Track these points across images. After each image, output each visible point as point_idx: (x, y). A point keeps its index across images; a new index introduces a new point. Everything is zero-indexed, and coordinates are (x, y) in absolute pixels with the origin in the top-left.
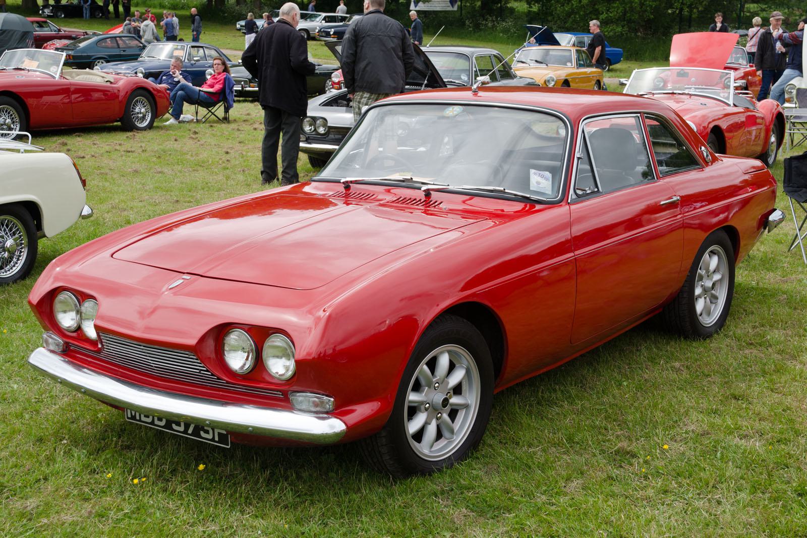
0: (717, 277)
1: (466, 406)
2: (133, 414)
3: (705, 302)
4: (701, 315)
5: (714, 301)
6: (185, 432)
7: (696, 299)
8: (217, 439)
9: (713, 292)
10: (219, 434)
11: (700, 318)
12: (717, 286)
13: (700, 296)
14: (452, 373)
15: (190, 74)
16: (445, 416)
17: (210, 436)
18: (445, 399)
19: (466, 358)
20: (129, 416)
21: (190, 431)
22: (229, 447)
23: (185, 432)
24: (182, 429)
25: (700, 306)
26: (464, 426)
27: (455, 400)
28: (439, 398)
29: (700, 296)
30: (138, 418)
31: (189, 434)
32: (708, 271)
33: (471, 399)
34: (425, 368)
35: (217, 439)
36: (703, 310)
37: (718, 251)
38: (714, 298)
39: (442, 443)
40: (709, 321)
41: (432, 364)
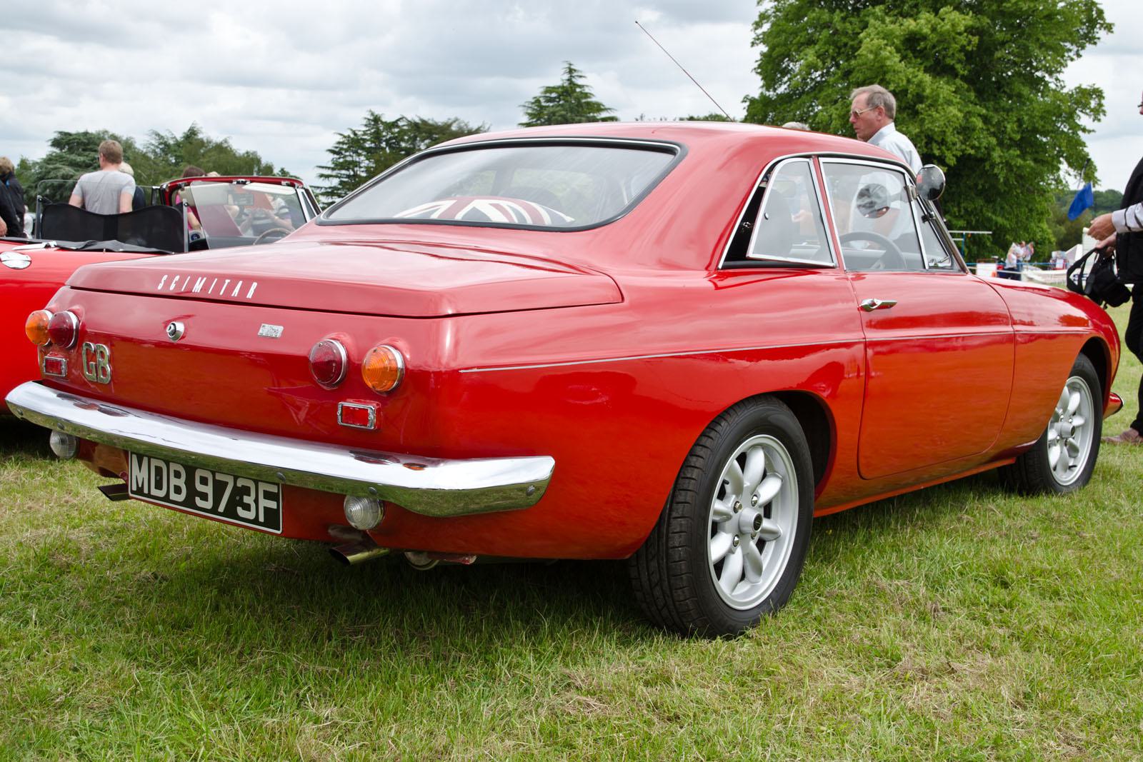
0: (1078, 421)
2: (140, 486)
5: (1074, 455)
8: (261, 519)
11: (1054, 473)
12: (1078, 434)
14: (760, 480)
16: (753, 544)
17: (250, 515)
18: (753, 508)
20: (134, 488)
21: (221, 509)
22: (279, 532)
25: (1055, 455)
26: (776, 562)
29: (1054, 442)
30: (146, 491)
32: (1065, 409)
33: (785, 525)
34: (736, 464)
35: (261, 519)
36: (1057, 463)
37: (1081, 386)
38: (1073, 450)
39: (743, 587)
40: (1066, 478)
41: (742, 460)
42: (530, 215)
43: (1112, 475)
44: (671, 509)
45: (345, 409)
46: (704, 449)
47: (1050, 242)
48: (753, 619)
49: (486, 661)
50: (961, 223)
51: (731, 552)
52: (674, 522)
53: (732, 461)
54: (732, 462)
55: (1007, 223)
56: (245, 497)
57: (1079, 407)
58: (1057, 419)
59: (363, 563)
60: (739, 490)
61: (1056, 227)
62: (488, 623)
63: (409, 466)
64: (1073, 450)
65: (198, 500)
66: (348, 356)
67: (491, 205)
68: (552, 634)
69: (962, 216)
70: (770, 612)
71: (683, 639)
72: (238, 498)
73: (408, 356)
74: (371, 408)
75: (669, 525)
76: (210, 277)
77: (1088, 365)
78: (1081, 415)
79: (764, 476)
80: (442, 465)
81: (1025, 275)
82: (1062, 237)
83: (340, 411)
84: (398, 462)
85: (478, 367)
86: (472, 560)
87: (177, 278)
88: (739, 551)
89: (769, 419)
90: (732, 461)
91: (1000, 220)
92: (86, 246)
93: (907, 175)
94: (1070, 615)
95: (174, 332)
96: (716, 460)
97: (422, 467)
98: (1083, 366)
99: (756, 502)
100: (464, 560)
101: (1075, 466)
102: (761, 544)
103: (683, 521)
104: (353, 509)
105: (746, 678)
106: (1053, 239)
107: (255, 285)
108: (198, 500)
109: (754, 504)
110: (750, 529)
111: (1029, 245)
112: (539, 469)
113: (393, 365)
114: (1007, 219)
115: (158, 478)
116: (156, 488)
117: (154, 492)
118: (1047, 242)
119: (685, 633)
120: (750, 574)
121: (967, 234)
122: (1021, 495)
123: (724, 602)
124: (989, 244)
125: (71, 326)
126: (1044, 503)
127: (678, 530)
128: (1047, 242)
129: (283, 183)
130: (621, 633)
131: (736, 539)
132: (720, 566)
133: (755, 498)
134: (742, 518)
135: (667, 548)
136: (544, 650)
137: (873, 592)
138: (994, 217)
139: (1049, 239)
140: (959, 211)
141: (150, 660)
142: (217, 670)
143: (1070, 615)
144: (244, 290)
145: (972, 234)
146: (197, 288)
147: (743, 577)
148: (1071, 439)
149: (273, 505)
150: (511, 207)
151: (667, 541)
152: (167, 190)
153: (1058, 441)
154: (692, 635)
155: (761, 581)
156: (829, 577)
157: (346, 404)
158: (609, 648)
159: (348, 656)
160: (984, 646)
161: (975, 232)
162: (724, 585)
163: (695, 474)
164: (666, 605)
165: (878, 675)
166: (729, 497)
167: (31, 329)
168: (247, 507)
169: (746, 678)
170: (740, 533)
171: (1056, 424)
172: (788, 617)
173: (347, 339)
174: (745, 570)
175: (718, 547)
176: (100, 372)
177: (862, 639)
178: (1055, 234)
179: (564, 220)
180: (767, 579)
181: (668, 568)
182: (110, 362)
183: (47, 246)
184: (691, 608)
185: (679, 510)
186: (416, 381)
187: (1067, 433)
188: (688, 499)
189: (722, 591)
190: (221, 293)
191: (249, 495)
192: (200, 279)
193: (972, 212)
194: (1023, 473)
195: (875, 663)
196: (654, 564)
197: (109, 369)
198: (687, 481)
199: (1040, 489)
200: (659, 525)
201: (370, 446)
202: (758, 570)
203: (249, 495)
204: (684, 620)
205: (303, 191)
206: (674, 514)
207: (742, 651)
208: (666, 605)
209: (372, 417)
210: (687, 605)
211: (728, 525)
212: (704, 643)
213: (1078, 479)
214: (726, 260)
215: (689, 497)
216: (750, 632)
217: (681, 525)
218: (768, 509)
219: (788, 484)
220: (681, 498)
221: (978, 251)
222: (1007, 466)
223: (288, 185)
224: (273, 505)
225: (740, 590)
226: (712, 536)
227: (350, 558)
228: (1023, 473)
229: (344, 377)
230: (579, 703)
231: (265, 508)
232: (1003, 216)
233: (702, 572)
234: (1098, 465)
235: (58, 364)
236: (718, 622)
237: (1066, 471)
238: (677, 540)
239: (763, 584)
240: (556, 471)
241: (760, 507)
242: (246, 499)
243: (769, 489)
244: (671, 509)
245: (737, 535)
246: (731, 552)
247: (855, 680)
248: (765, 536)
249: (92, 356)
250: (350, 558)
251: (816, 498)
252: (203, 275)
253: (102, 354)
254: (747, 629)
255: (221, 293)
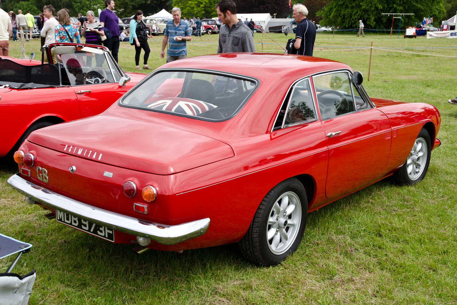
0: (420, 154)
1: (293, 225)
2: (61, 218)
3: (413, 167)
4: (410, 174)
6: (89, 230)
7: (408, 166)
8: (107, 236)
9: (418, 162)
10: (108, 233)
12: (421, 159)
13: (410, 164)
15: (83, 23)
16: (284, 230)
17: (103, 234)
18: (284, 222)
19: (296, 199)
20: (59, 219)
21: (92, 230)
22: (113, 242)
23: (89, 230)
24: (87, 228)
25: (410, 169)
26: (292, 235)
27: (289, 222)
28: (282, 220)
29: (410, 164)
30: (63, 220)
31: (91, 232)
32: (415, 150)
33: (296, 221)
34: (278, 204)
35: (107, 236)
39: (281, 245)
40: (414, 177)
41: (280, 202)
42: (199, 107)
43: (435, 171)
44: (253, 224)
45: (136, 206)
46: (265, 202)
47: (443, 12)
48: (284, 257)
49: (188, 281)
50: (401, 8)
51: (276, 234)
52: (254, 229)
53: (276, 203)
54: (276, 203)
55: (422, 7)
56: (100, 228)
57: (421, 148)
58: (412, 155)
59: (143, 253)
60: (279, 212)
61: (447, 4)
62: (188, 264)
63: (159, 227)
64: (418, 166)
65: (83, 226)
66: (137, 188)
67: (186, 104)
68: (210, 268)
69: (401, 5)
70: (290, 254)
71: (258, 268)
72: (98, 228)
73: (157, 189)
74: (145, 206)
75: (252, 229)
76: (84, 149)
77: (426, 132)
78: (422, 151)
79: (289, 204)
80: (171, 227)
81: (428, 34)
82: (449, 9)
83: (134, 207)
84: (155, 225)
85: (183, 192)
86: (182, 252)
87: (71, 147)
88: (279, 233)
89: (290, 186)
90: (276, 203)
91: (419, 6)
92: (22, 86)
93: (349, 73)
94: (401, 251)
95: (72, 170)
96: (269, 206)
97: (163, 228)
98: (423, 133)
99: (285, 215)
100: (179, 252)
101: (419, 172)
102: (287, 230)
103: (257, 229)
104: (140, 240)
105: (279, 286)
106: (445, 11)
107: (101, 155)
108: (83, 226)
109: (284, 216)
110: (283, 226)
111: (431, 18)
112: (203, 223)
113: (153, 193)
114: (422, 5)
115: (67, 216)
116: (67, 220)
117: (66, 221)
118: (442, 12)
119: (258, 265)
120: (283, 240)
121: (402, 15)
122: (396, 186)
123: (272, 253)
124: (413, 17)
125: (32, 159)
126: (404, 190)
127: (256, 232)
128: (442, 12)
129: (98, 48)
130: (236, 265)
131: (278, 229)
132: (271, 241)
133: (285, 214)
134: (280, 222)
135: (252, 238)
136: (208, 275)
137: (330, 241)
138: (416, 5)
139: (443, 11)
140: (400, 2)
141: (69, 283)
142: (92, 289)
143: (401, 251)
144: (98, 156)
145: (405, 15)
146: (80, 152)
147: (281, 241)
148: (418, 162)
149: (111, 232)
150: (194, 107)
151: (252, 235)
152: (49, 48)
153: (412, 163)
154: (261, 266)
155: (287, 242)
156: (315, 234)
157: (137, 204)
158: (230, 272)
159: (139, 281)
160: (367, 268)
161: (406, 14)
162: (273, 247)
163: (262, 211)
164: (251, 256)
165: (327, 282)
166: (275, 215)
167: (16, 158)
168: (101, 232)
169: (279, 286)
170: (279, 227)
171: (411, 157)
172: (296, 256)
173: (136, 181)
174: (279, 241)
175: (270, 234)
176: (44, 178)
177: (323, 266)
178: (446, 8)
179: (213, 107)
180: (289, 241)
181: (252, 245)
182: (48, 175)
183: (5, 87)
184: (260, 257)
185: (256, 225)
186: (160, 199)
187: (415, 160)
188: (259, 221)
189: (272, 250)
190: (89, 156)
191: (102, 228)
192: (80, 149)
193: (406, 3)
194: (398, 178)
195: (326, 277)
196: (247, 243)
197: (47, 172)
198: (259, 214)
199: (403, 183)
200: (249, 230)
201: (145, 219)
202: (286, 238)
203: (102, 228)
204: (258, 261)
205: (107, 53)
206: (254, 226)
207: (277, 272)
208: (251, 256)
209: (146, 210)
210: (259, 257)
211: (274, 225)
212: (266, 270)
213: (419, 178)
214: (274, 127)
215: (259, 220)
216: (282, 263)
217: (257, 230)
218: (290, 217)
219: (298, 208)
220: (256, 220)
221: (408, 21)
222: (391, 176)
223: (100, 49)
224: (111, 232)
225: (278, 247)
226: (268, 230)
227: (139, 252)
228: (398, 178)
229: (137, 195)
230: (220, 301)
231: (108, 233)
232: (421, 4)
233: (264, 243)
234: (429, 168)
235: (27, 172)
236: (271, 260)
237: (415, 174)
238: (255, 235)
239: (288, 243)
240: (211, 223)
241: (287, 216)
242: (101, 229)
243: (290, 209)
244: (253, 224)
245: (278, 228)
246: (276, 234)
247: (318, 284)
248: (289, 226)
249: (40, 172)
250: (139, 252)
251: (309, 208)
252: (82, 147)
253: (45, 172)
254: (281, 262)
255: (89, 156)
